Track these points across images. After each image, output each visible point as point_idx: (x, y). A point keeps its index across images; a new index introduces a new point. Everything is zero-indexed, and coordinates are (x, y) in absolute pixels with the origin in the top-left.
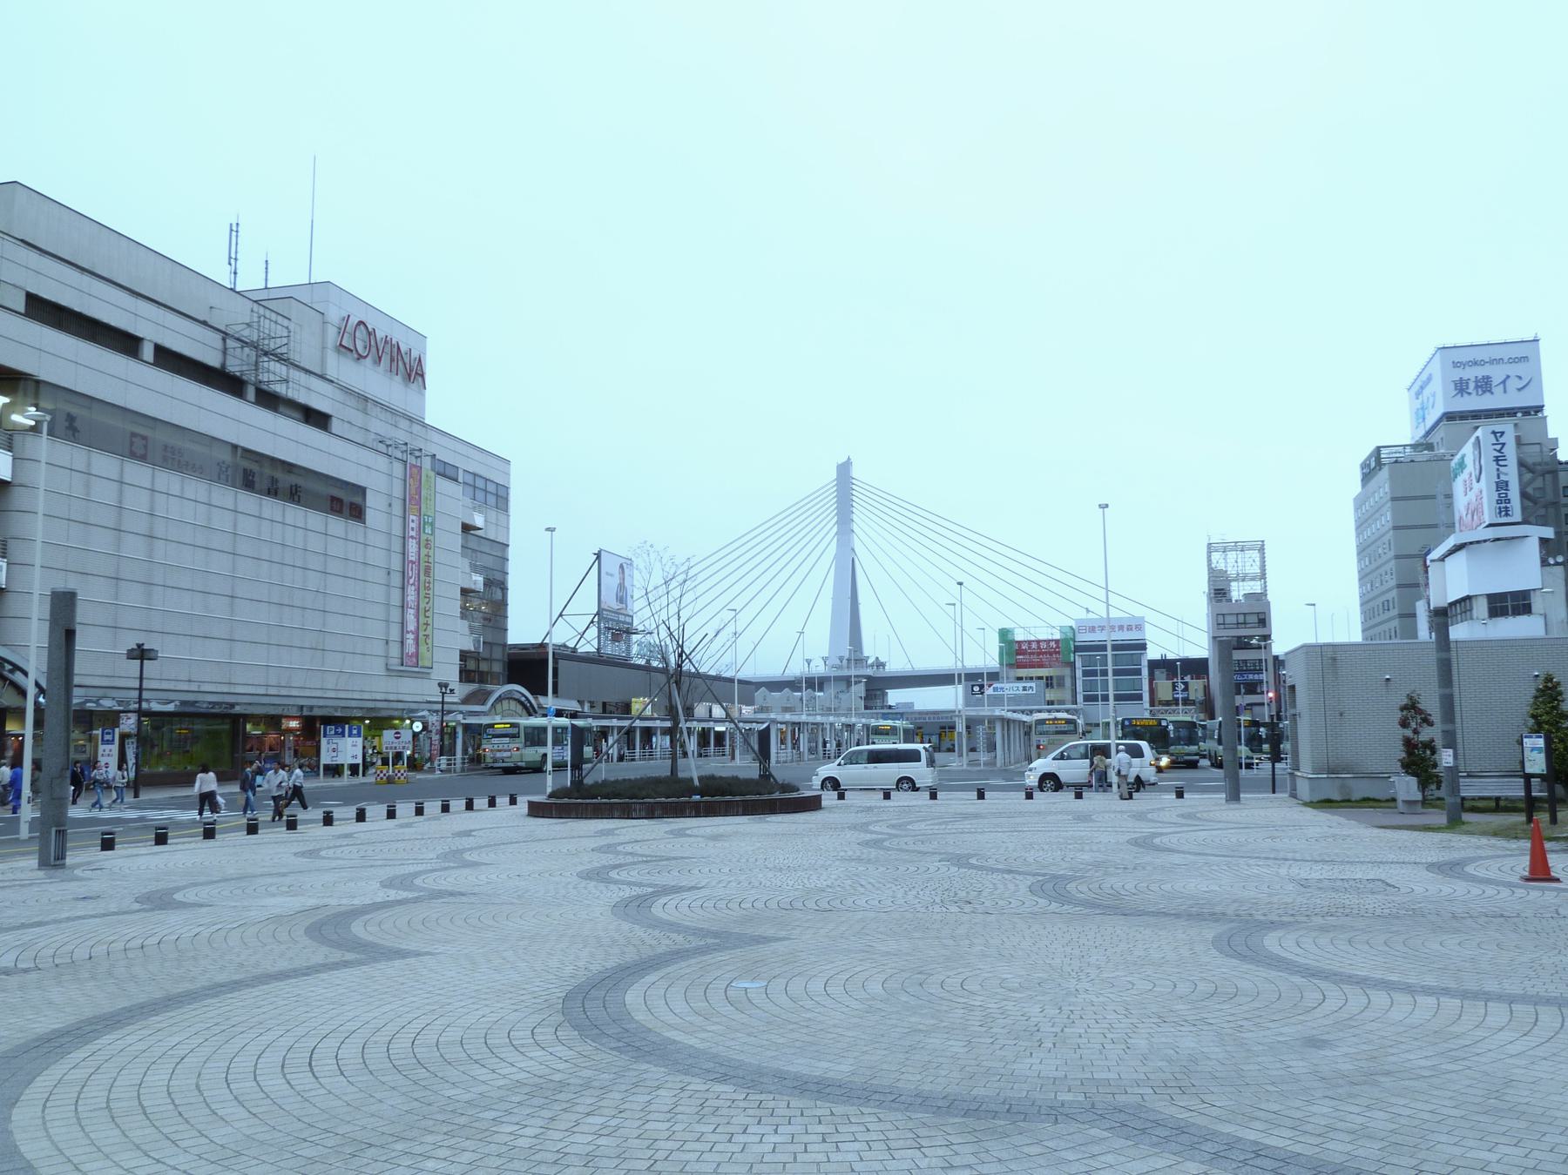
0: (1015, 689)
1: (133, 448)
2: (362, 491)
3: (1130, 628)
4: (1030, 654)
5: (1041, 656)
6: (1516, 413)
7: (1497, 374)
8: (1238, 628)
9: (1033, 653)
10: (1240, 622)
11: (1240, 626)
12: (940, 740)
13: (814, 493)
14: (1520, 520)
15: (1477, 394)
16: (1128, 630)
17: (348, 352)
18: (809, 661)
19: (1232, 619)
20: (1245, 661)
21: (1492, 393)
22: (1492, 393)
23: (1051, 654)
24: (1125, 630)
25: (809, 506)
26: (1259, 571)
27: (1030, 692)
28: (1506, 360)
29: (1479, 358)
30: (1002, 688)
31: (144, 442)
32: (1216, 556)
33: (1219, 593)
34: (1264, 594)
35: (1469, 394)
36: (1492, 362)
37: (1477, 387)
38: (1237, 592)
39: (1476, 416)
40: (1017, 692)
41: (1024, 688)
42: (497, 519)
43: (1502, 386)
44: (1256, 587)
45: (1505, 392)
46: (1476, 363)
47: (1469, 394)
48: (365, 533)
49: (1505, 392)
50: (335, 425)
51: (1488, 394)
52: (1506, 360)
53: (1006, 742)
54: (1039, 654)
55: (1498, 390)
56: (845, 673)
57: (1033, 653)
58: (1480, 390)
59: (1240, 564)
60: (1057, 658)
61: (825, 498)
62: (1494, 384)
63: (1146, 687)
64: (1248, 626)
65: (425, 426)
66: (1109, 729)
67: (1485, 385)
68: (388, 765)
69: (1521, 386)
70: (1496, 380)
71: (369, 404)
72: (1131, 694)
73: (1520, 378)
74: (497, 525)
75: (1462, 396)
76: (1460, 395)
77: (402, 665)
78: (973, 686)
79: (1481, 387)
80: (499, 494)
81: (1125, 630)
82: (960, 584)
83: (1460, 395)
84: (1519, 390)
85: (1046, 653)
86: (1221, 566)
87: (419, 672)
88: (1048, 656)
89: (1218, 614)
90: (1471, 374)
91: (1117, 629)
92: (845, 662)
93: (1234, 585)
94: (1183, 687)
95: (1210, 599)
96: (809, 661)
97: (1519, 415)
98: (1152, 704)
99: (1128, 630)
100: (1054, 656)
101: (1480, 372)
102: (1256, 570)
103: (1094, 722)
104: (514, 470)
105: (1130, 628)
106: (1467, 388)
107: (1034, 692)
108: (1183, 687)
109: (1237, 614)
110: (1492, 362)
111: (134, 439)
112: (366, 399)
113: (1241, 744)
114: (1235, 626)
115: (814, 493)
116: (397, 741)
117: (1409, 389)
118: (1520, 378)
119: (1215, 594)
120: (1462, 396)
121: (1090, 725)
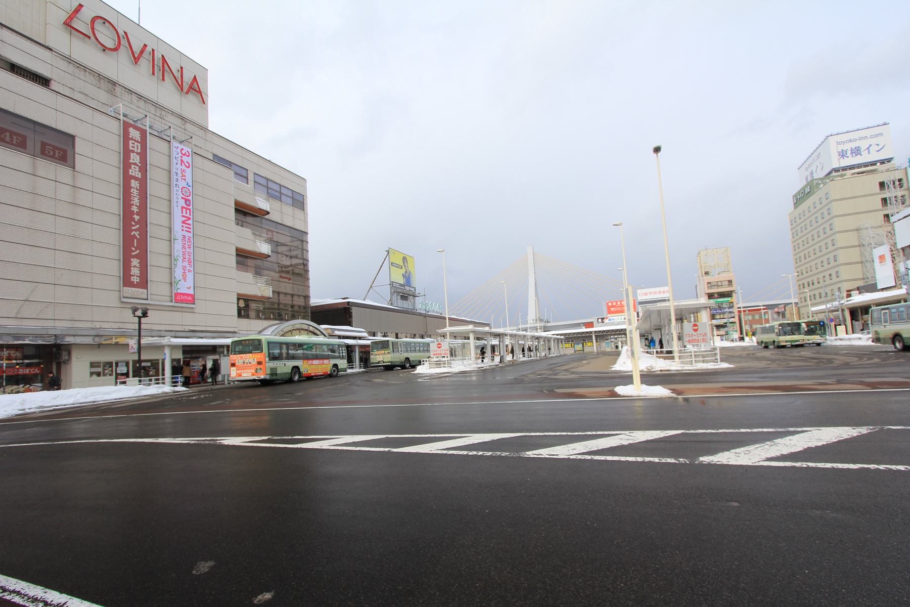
2: (72, 138)
4: (617, 307)
6: (876, 164)
7: (863, 145)
12: (583, 346)
15: (852, 156)
17: (87, 39)
21: (861, 155)
22: (861, 155)
24: (658, 293)
28: (869, 137)
29: (852, 138)
35: (848, 157)
36: (861, 139)
37: (852, 153)
39: (851, 168)
42: (293, 214)
43: (867, 150)
45: (869, 153)
46: (851, 141)
47: (848, 157)
48: (74, 176)
49: (869, 153)
50: (53, 85)
51: (859, 156)
52: (869, 137)
53: (161, 308)
55: (864, 153)
56: (535, 325)
58: (854, 154)
62: (862, 150)
65: (205, 129)
66: (222, 346)
67: (857, 151)
68: (764, 319)
69: (879, 149)
71: (116, 88)
73: (878, 145)
74: (293, 217)
75: (843, 158)
76: (842, 158)
77: (172, 301)
78: (598, 319)
79: (855, 152)
80: (282, 191)
83: (842, 158)
84: (878, 151)
87: (174, 306)
90: (848, 147)
91: (658, 293)
92: (535, 321)
97: (878, 164)
101: (853, 145)
104: (309, 185)
106: (846, 154)
110: (861, 139)
112: (114, 84)
116: (695, 333)
117: (799, 169)
118: (878, 145)
120: (843, 158)
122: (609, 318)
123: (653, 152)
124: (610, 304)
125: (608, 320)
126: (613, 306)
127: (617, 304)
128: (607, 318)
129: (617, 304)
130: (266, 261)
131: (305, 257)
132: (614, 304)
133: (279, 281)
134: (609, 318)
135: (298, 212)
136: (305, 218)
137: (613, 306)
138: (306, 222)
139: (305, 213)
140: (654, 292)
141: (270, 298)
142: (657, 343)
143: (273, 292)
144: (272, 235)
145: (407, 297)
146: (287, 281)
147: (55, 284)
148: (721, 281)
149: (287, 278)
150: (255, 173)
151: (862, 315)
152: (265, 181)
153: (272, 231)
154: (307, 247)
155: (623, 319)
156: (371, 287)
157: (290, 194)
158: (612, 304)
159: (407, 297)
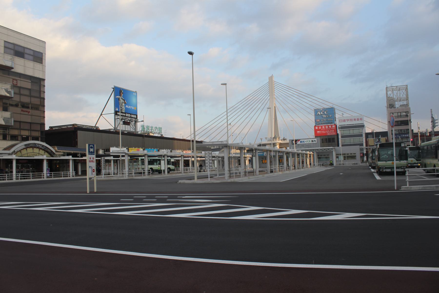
0: (309, 141)
1: (14, 83)
3: (358, 120)
4: (322, 130)
5: (326, 131)
8: (398, 118)
9: (323, 130)
10: (399, 115)
11: (399, 117)
13: (259, 89)
14: (164, 161)
16: (357, 120)
18: (261, 139)
19: (396, 114)
20: (401, 130)
23: (330, 130)
24: (356, 120)
25: (257, 94)
26: (405, 96)
27: (315, 142)
30: (304, 141)
31: (16, 81)
32: (389, 92)
33: (391, 106)
34: (407, 105)
38: (397, 105)
40: (310, 143)
41: (312, 141)
44: (405, 103)
54: (325, 130)
57: (323, 130)
59: (398, 94)
60: (332, 132)
61: (262, 89)
63: (364, 141)
64: (402, 117)
70: (305, 141)
72: (359, 143)
81: (356, 120)
82: (191, 53)
85: (328, 130)
86: (392, 95)
88: (329, 131)
89: (390, 113)
91: (353, 120)
93: (396, 103)
94: (378, 140)
95: (387, 108)
96: (261, 139)
98: (367, 146)
99: (357, 120)
100: (331, 131)
102: (400, 113)
103: (339, 153)
105: (358, 120)
107: (316, 142)
108: (378, 140)
109: (398, 113)
111: (13, 81)
113: (365, 154)
114: (397, 117)
115: (259, 89)
119: (389, 106)
121: (338, 154)
122: (301, 140)
123: (46, 80)
124: (317, 128)
125: (299, 142)
126: (319, 130)
127: (322, 128)
128: (299, 140)
129: (322, 128)
130: (11, 100)
131: (42, 96)
132: (320, 128)
133: (21, 114)
134: (301, 140)
135: (38, 65)
136: (43, 69)
137: (319, 130)
138: (44, 72)
139: (43, 65)
140: (350, 120)
141: (12, 126)
142: (124, 174)
143: (14, 121)
144: (17, 82)
145: (129, 122)
146: (27, 113)
147: (39, 70)
148: (400, 112)
149: (27, 112)
150: (5, 41)
151: (344, 156)
152: (13, 45)
153: (16, 80)
154: (44, 89)
155: (311, 141)
156: (101, 115)
157: (32, 53)
158: (318, 128)
159: (129, 122)
